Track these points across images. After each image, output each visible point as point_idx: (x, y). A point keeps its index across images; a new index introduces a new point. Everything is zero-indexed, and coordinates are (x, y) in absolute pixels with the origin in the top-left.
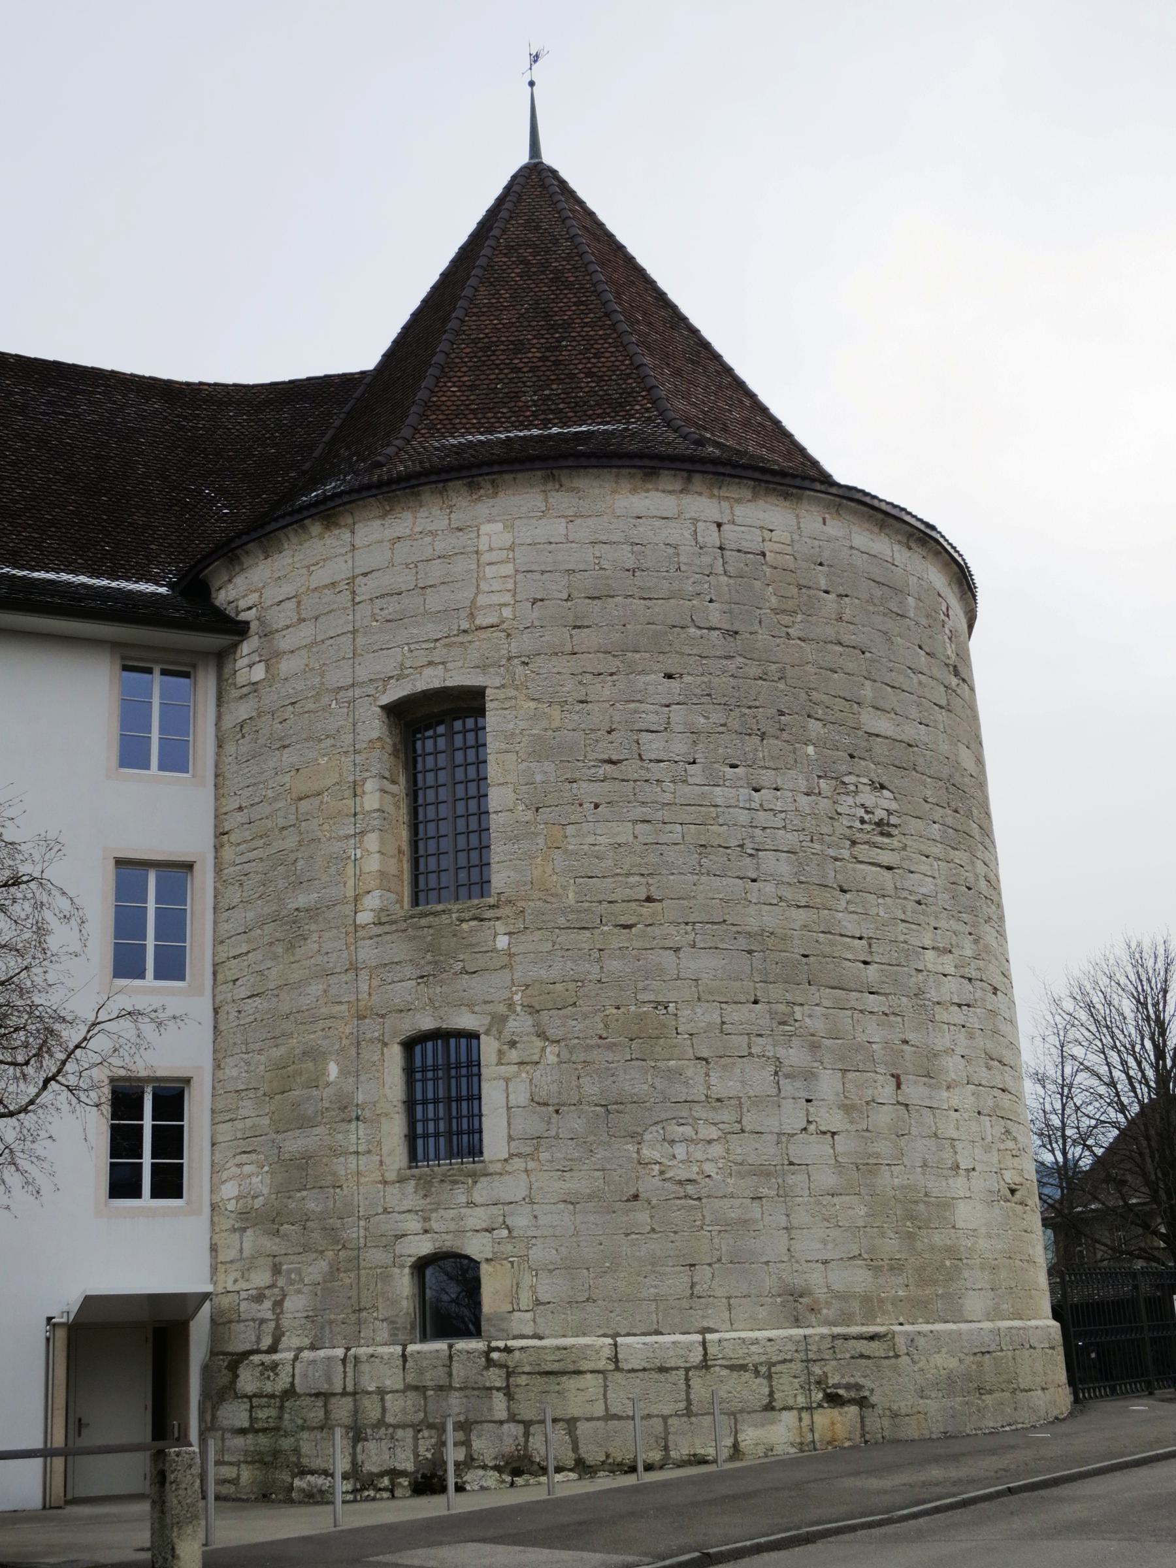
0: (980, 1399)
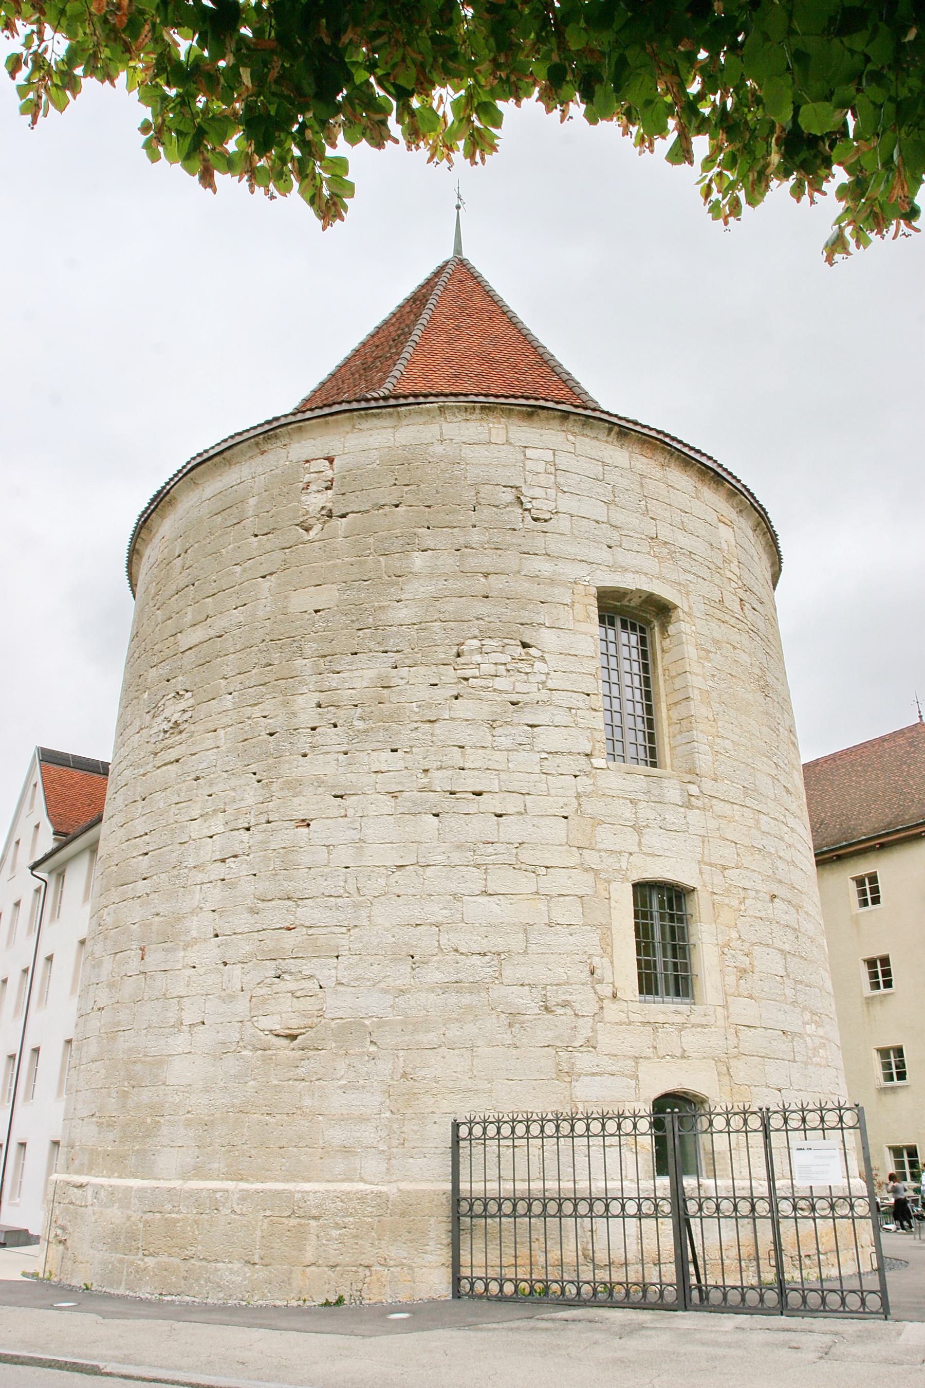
0: (143, 1260)
